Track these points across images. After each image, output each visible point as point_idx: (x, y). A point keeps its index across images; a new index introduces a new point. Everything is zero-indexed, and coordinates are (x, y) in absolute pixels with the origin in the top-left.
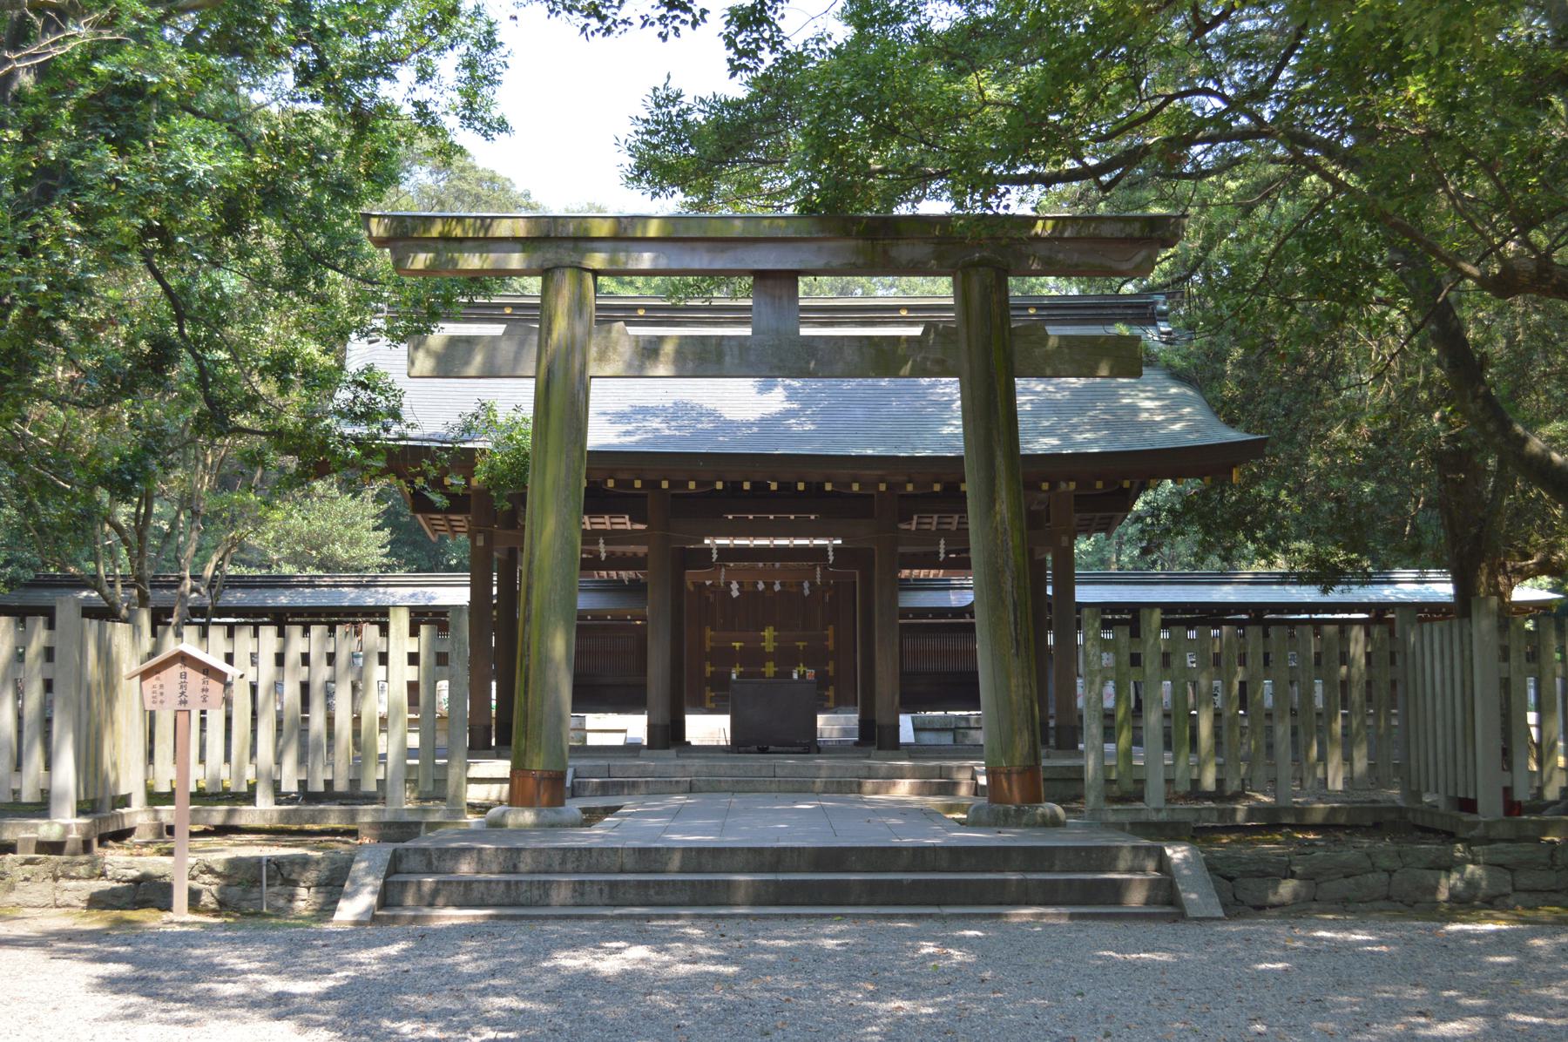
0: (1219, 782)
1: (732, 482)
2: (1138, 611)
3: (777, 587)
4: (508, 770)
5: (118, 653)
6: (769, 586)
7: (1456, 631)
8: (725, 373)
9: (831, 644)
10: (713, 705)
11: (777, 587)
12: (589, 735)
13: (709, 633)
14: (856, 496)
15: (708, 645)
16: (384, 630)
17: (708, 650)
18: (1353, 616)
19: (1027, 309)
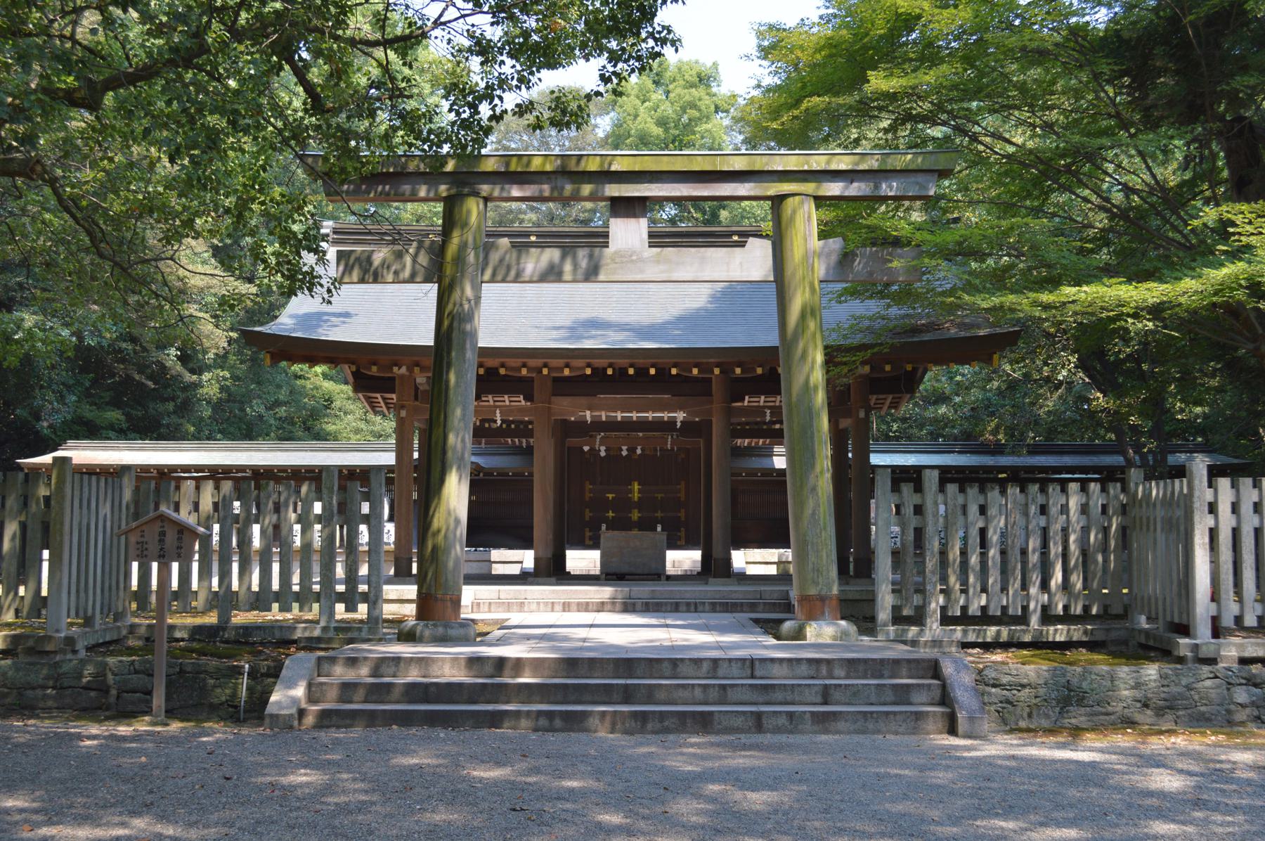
0: (1066, 608)
1: (620, 369)
2: (921, 472)
3: (639, 451)
4: (416, 593)
5: (448, 498)
6: (632, 450)
7: (102, 484)
8: (749, 285)
9: (682, 496)
10: (591, 543)
11: (639, 451)
12: (494, 565)
13: (589, 487)
14: (695, 379)
15: (588, 495)
16: (919, 488)
17: (587, 499)
18: (1089, 476)
19: (529, 236)
